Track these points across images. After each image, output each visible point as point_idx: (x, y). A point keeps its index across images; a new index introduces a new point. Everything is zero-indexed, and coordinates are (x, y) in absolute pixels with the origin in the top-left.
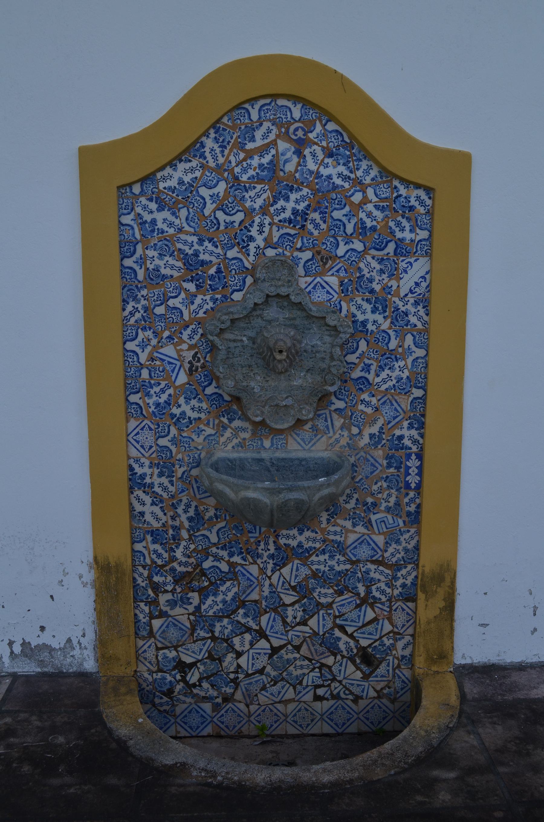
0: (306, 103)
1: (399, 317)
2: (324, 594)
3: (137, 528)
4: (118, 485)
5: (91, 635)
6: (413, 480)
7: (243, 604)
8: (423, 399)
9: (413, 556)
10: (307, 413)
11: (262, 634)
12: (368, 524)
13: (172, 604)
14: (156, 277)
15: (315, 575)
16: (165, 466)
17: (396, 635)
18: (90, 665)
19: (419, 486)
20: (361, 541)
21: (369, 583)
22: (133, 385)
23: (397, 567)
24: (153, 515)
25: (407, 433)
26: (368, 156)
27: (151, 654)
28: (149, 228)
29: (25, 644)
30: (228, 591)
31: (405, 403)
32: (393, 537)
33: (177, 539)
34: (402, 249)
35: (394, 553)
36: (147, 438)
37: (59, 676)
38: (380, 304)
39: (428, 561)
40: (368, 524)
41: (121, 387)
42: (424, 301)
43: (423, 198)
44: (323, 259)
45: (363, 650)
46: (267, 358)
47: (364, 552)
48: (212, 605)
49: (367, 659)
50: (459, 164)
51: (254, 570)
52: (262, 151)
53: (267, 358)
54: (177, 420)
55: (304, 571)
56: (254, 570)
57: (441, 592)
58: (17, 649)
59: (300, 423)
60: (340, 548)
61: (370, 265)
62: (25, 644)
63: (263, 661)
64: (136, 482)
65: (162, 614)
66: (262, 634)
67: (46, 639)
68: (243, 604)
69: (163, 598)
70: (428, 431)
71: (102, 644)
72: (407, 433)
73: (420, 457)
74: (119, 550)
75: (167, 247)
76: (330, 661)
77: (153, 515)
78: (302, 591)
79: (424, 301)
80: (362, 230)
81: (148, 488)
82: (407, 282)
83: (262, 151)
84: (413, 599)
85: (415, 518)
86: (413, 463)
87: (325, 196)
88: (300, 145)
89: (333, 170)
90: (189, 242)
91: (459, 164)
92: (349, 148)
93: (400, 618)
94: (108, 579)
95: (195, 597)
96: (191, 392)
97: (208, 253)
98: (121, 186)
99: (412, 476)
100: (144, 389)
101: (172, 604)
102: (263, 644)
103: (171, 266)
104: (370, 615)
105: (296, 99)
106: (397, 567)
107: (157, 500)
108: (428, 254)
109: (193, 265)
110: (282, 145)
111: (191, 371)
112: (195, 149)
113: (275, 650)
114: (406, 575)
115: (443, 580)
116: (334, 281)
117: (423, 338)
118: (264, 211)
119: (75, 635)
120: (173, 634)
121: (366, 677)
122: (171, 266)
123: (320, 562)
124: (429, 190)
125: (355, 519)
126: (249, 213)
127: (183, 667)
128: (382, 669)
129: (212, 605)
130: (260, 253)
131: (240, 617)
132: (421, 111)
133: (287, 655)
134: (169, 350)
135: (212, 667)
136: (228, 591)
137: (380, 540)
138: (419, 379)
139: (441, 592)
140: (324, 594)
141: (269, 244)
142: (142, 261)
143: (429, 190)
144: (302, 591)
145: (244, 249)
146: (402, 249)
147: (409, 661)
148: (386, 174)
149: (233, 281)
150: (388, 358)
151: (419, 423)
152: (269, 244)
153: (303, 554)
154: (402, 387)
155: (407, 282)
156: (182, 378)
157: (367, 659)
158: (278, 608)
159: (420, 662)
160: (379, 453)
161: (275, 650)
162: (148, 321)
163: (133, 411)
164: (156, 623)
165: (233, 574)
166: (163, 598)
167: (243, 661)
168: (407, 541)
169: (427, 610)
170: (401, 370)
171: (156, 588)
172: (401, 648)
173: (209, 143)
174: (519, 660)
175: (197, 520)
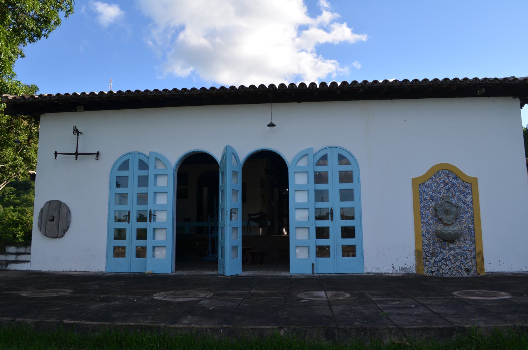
0: (449, 170)
1: (467, 205)
2: (458, 257)
3: (424, 245)
4: (419, 236)
5: (415, 265)
6: (473, 234)
7: (443, 259)
8: (473, 220)
9: (475, 249)
10: (454, 221)
11: (447, 265)
12: (466, 243)
13: (430, 259)
14: (425, 199)
15: (456, 253)
16: (428, 232)
17: (473, 265)
18: (414, 272)
19: (474, 236)
20: (465, 246)
21: (467, 255)
22: (422, 218)
23: (472, 252)
24: (426, 242)
25: (471, 226)
26: (460, 178)
27: (426, 269)
28: (424, 191)
29: (402, 267)
30: (440, 256)
31: (470, 220)
32: (470, 246)
33: (430, 246)
34: (467, 194)
35: (471, 249)
36: (425, 227)
37: (409, 274)
38: (464, 203)
39: (478, 250)
40: (466, 243)
41: (420, 218)
42: (472, 202)
43: (469, 186)
44: (454, 196)
45: (467, 269)
46: (447, 212)
47: (465, 249)
48: (437, 259)
49: (468, 270)
50: (476, 179)
51: (445, 252)
52: (442, 178)
53: (447, 212)
54: (430, 224)
55: (454, 252)
56: (445, 252)
57: (481, 256)
58: (401, 268)
59: (452, 223)
60: (461, 248)
61: (462, 196)
62: (402, 267)
63: (447, 271)
64: (423, 235)
65: (428, 261)
66: (447, 265)
67: (406, 266)
68: (443, 259)
69: (428, 258)
70: (475, 225)
71: (417, 266)
72: (471, 226)
73: (474, 230)
74: (420, 248)
75: (427, 194)
76: (460, 271)
77: (426, 242)
78: (454, 256)
79: (472, 202)
80: (460, 191)
81: (425, 236)
82: (468, 199)
83: (442, 178)
84: (475, 258)
85: (474, 242)
86: (473, 231)
87: (453, 185)
88: (448, 177)
89: (454, 181)
90: (430, 193)
91: (476, 179)
92: (456, 177)
93: (473, 262)
94: (418, 254)
95: (434, 258)
96: (432, 219)
97: (434, 195)
98: (420, 185)
99: (473, 233)
100: (424, 218)
101: (430, 259)
102: (447, 267)
103: (428, 197)
104: (467, 261)
105: (447, 170)
106: (472, 252)
107: (427, 239)
108: (472, 194)
109: (431, 197)
110: (445, 177)
111: (432, 215)
112: (431, 178)
113: (450, 269)
114: (474, 253)
115: (480, 254)
116: (456, 199)
117: (472, 209)
118: (443, 188)
119: (412, 265)
120: (430, 265)
121: (468, 274)
122: (428, 197)
123: (457, 251)
124: (471, 184)
125: (463, 242)
126: (441, 188)
127: (432, 272)
128: (471, 273)
129: (437, 259)
130: (443, 195)
131: (443, 261)
132: (468, 169)
133: (452, 269)
134: (428, 212)
135: (438, 272)
136: (440, 256)
137: (468, 246)
138: (472, 216)
139: (481, 256)
140: (458, 257)
141: (444, 193)
142: (423, 196)
143: (471, 184)
144: (454, 256)
145: (440, 194)
146: (467, 194)
147: (476, 271)
148: (463, 181)
149: (438, 200)
150: (466, 212)
151: (473, 224)
152: (444, 193)
153: (454, 249)
154: (470, 217)
155: (468, 199)
156: (430, 216)
157: (468, 270)
158: (450, 260)
159: (478, 270)
160: (466, 230)
161: (450, 269)
162: (424, 206)
163: (423, 222)
164: (427, 263)
165: (441, 253)
166: (428, 258)
167: (444, 271)
168: (473, 246)
169: (479, 260)
170: (469, 214)
171: (427, 256)
172: (474, 268)
173: (433, 177)
174: (497, 271)
175: (434, 242)
